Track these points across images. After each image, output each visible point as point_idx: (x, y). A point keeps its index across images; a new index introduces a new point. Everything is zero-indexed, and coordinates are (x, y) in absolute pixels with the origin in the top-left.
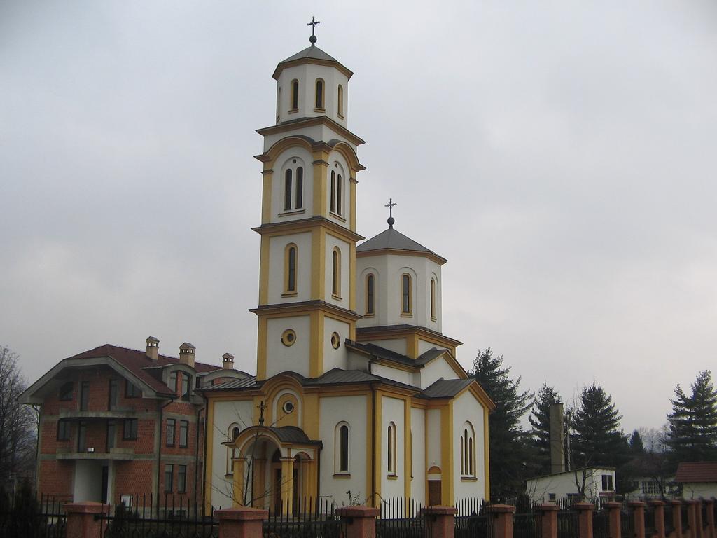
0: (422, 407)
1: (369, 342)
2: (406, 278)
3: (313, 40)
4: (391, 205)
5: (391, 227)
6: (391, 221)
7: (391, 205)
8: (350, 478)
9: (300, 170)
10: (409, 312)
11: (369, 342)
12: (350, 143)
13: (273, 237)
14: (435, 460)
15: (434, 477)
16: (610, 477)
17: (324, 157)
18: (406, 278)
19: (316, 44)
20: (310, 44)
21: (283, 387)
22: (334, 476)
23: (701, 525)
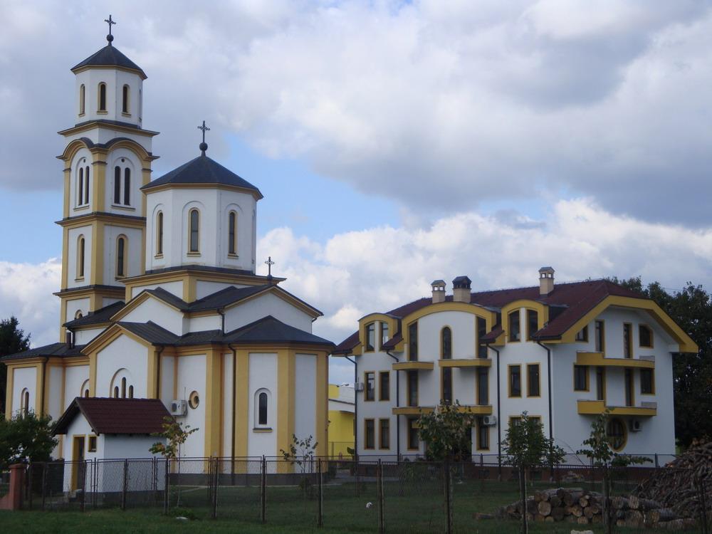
9: (88, 168)
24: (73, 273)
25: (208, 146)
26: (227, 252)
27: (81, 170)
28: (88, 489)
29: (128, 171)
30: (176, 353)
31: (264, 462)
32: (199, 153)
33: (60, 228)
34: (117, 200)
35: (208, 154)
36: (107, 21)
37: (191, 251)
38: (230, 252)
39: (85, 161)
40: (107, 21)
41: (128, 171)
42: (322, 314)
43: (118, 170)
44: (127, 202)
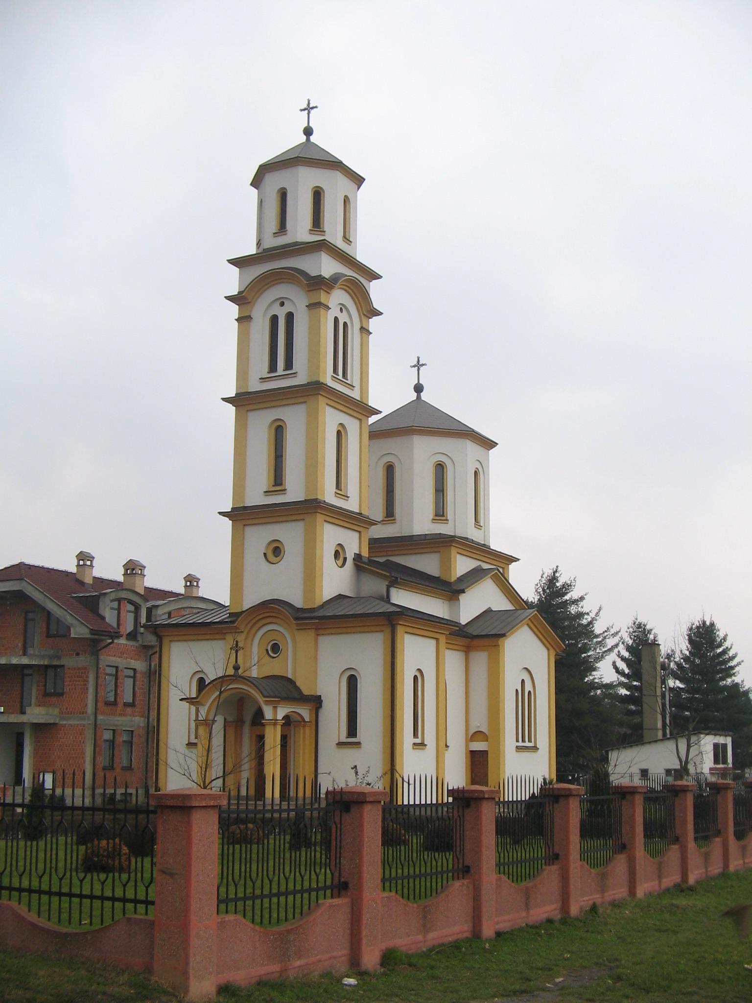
2: (440, 468)
3: (308, 132)
5: (419, 397)
6: (419, 389)
7: (418, 365)
9: (290, 317)
16: (725, 746)
18: (440, 468)
37: (436, 515)
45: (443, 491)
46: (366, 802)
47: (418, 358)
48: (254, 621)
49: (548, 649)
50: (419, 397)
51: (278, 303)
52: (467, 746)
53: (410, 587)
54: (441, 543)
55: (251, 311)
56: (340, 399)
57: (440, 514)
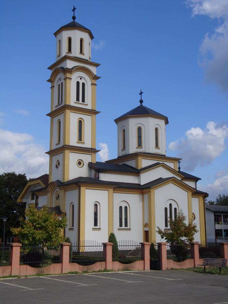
0: (138, 193)
1: (159, 162)
2: (139, 129)
3: (74, 18)
4: (141, 93)
5: (141, 104)
6: (141, 101)
7: (141, 93)
8: (73, 230)
9: (62, 83)
10: (141, 146)
11: (159, 162)
12: (57, 67)
13: (55, 117)
14: (146, 221)
15: (146, 229)
16: (9, 242)
17: (68, 75)
18: (139, 129)
19: (76, 20)
20: (72, 20)
21: (55, 188)
22: (69, 229)
23: (127, 271)
24: (56, 141)
25: (76, 19)
26: (155, 146)
27: (59, 85)
28: (80, 251)
29: (83, 84)
30: (143, 192)
31: (190, 233)
32: (139, 104)
33: (49, 118)
34: (78, 99)
35: (143, 104)
36: (141, 92)
37: (138, 146)
38: (156, 146)
39: (60, 80)
40: (141, 92)
41: (83, 84)
42: (200, 179)
43: (78, 83)
44: (83, 100)
45: (141, 137)
46: (216, 243)
47: (141, 90)
48: (52, 189)
49: (187, 192)
50: (141, 104)
51: (80, 78)
52: (143, 229)
53: (117, 173)
54: (135, 156)
55: (52, 84)
56: (79, 110)
57: (140, 144)
